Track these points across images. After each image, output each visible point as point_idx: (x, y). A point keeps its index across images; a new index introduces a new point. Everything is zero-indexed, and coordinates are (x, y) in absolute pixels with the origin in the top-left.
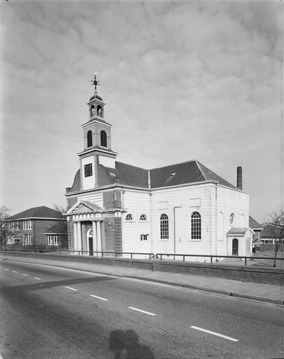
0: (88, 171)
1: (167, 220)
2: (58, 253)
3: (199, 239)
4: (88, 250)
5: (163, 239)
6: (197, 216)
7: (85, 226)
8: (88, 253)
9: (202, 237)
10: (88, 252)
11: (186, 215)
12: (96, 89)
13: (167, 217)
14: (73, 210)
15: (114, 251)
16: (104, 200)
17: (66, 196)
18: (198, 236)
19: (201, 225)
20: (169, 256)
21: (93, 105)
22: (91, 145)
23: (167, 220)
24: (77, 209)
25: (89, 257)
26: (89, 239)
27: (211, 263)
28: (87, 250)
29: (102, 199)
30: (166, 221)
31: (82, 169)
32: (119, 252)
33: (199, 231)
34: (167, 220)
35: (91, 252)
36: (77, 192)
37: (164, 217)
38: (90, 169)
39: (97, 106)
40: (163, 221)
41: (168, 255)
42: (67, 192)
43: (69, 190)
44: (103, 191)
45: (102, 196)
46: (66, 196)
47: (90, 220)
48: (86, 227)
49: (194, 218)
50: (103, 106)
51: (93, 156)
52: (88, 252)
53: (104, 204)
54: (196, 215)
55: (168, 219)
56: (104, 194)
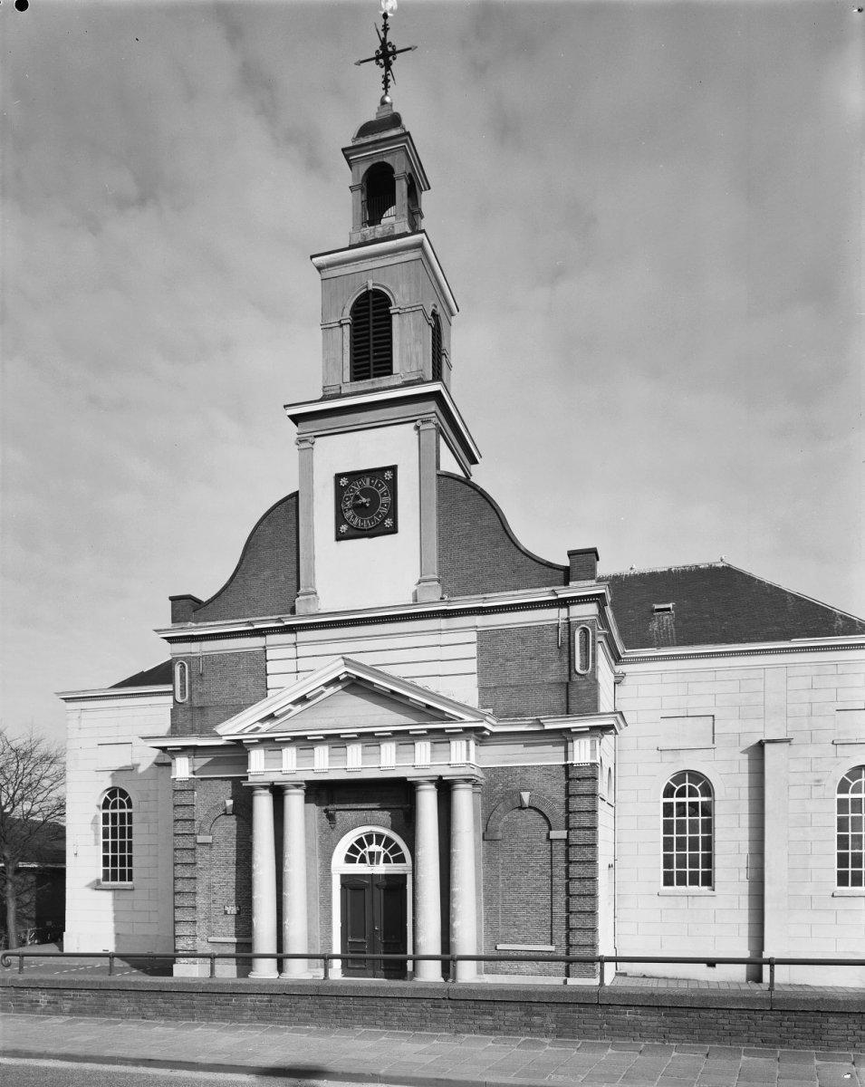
0: (366, 505)
1: (130, 810)
2: (100, 970)
3: (127, 883)
4: (337, 950)
5: (675, 888)
6: (120, 801)
7: (317, 808)
8: (337, 964)
9: (135, 875)
10: (336, 957)
11: (818, 781)
12: (386, 88)
13: (129, 802)
14: (271, 717)
15: (552, 948)
16: (482, 672)
17: (171, 640)
18: (123, 872)
19: (134, 832)
20: (717, 965)
21: (387, 160)
22: (386, 369)
23: (126, 811)
24: (299, 708)
25: (234, 985)
26: (343, 885)
27: (324, 979)
28: (330, 946)
29: (473, 666)
30: (122, 815)
31: (311, 496)
32: (579, 956)
33: (126, 854)
34: (126, 811)
35: (245, 954)
36: (250, 623)
37: (118, 798)
38: (386, 500)
39: (385, 183)
40: (114, 815)
41: (711, 963)
42: (174, 620)
43: (185, 607)
44: (479, 620)
45: (472, 650)
46: (171, 640)
47: (409, 774)
48: (331, 818)
49: (112, 808)
50: (421, 191)
51: (413, 425)
52: (336, 957)
53: (483, 689)
54: (687, 784)
55: (130, 806)
56: (487, 640)
